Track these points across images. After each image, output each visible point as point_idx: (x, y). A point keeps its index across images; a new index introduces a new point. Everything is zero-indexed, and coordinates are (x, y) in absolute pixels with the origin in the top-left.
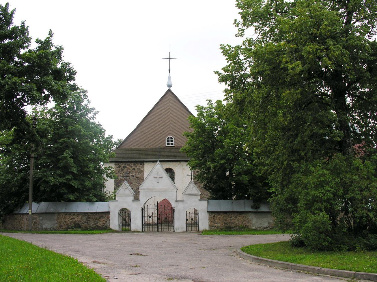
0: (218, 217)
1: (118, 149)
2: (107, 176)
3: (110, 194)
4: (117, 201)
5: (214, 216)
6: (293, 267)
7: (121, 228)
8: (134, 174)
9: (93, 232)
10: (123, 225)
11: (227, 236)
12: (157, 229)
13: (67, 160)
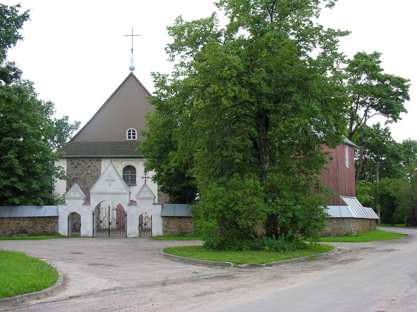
0: (172, 222)
1: (71, 142)
2: (57, 176)
3: (60, 196)
4: (67, 205)
5: (169, 221)
6: (183, 259)
7: (71, 233)
8: (89, 172)
9: (40, 237)
10: (73, 231)
11: (175, 241)
12: (108, 235)
13: (11, 161)
